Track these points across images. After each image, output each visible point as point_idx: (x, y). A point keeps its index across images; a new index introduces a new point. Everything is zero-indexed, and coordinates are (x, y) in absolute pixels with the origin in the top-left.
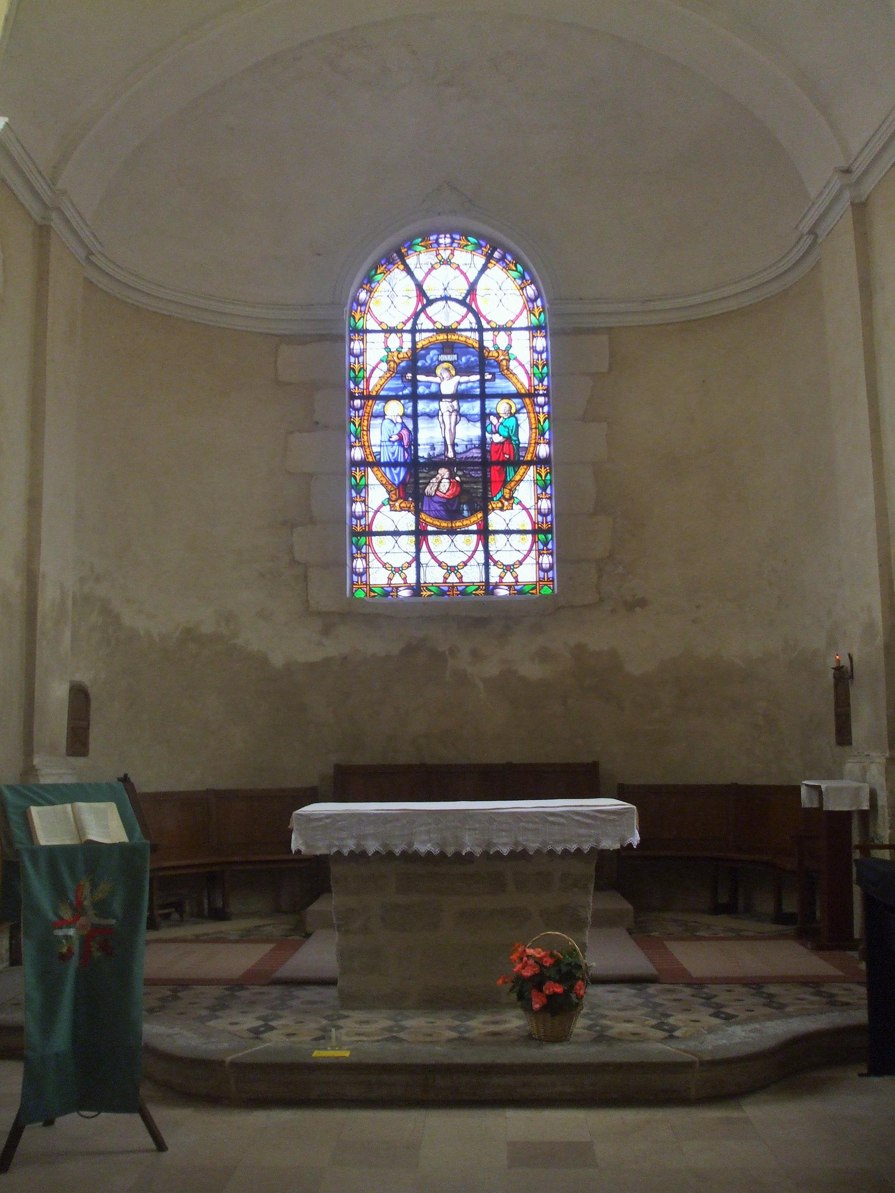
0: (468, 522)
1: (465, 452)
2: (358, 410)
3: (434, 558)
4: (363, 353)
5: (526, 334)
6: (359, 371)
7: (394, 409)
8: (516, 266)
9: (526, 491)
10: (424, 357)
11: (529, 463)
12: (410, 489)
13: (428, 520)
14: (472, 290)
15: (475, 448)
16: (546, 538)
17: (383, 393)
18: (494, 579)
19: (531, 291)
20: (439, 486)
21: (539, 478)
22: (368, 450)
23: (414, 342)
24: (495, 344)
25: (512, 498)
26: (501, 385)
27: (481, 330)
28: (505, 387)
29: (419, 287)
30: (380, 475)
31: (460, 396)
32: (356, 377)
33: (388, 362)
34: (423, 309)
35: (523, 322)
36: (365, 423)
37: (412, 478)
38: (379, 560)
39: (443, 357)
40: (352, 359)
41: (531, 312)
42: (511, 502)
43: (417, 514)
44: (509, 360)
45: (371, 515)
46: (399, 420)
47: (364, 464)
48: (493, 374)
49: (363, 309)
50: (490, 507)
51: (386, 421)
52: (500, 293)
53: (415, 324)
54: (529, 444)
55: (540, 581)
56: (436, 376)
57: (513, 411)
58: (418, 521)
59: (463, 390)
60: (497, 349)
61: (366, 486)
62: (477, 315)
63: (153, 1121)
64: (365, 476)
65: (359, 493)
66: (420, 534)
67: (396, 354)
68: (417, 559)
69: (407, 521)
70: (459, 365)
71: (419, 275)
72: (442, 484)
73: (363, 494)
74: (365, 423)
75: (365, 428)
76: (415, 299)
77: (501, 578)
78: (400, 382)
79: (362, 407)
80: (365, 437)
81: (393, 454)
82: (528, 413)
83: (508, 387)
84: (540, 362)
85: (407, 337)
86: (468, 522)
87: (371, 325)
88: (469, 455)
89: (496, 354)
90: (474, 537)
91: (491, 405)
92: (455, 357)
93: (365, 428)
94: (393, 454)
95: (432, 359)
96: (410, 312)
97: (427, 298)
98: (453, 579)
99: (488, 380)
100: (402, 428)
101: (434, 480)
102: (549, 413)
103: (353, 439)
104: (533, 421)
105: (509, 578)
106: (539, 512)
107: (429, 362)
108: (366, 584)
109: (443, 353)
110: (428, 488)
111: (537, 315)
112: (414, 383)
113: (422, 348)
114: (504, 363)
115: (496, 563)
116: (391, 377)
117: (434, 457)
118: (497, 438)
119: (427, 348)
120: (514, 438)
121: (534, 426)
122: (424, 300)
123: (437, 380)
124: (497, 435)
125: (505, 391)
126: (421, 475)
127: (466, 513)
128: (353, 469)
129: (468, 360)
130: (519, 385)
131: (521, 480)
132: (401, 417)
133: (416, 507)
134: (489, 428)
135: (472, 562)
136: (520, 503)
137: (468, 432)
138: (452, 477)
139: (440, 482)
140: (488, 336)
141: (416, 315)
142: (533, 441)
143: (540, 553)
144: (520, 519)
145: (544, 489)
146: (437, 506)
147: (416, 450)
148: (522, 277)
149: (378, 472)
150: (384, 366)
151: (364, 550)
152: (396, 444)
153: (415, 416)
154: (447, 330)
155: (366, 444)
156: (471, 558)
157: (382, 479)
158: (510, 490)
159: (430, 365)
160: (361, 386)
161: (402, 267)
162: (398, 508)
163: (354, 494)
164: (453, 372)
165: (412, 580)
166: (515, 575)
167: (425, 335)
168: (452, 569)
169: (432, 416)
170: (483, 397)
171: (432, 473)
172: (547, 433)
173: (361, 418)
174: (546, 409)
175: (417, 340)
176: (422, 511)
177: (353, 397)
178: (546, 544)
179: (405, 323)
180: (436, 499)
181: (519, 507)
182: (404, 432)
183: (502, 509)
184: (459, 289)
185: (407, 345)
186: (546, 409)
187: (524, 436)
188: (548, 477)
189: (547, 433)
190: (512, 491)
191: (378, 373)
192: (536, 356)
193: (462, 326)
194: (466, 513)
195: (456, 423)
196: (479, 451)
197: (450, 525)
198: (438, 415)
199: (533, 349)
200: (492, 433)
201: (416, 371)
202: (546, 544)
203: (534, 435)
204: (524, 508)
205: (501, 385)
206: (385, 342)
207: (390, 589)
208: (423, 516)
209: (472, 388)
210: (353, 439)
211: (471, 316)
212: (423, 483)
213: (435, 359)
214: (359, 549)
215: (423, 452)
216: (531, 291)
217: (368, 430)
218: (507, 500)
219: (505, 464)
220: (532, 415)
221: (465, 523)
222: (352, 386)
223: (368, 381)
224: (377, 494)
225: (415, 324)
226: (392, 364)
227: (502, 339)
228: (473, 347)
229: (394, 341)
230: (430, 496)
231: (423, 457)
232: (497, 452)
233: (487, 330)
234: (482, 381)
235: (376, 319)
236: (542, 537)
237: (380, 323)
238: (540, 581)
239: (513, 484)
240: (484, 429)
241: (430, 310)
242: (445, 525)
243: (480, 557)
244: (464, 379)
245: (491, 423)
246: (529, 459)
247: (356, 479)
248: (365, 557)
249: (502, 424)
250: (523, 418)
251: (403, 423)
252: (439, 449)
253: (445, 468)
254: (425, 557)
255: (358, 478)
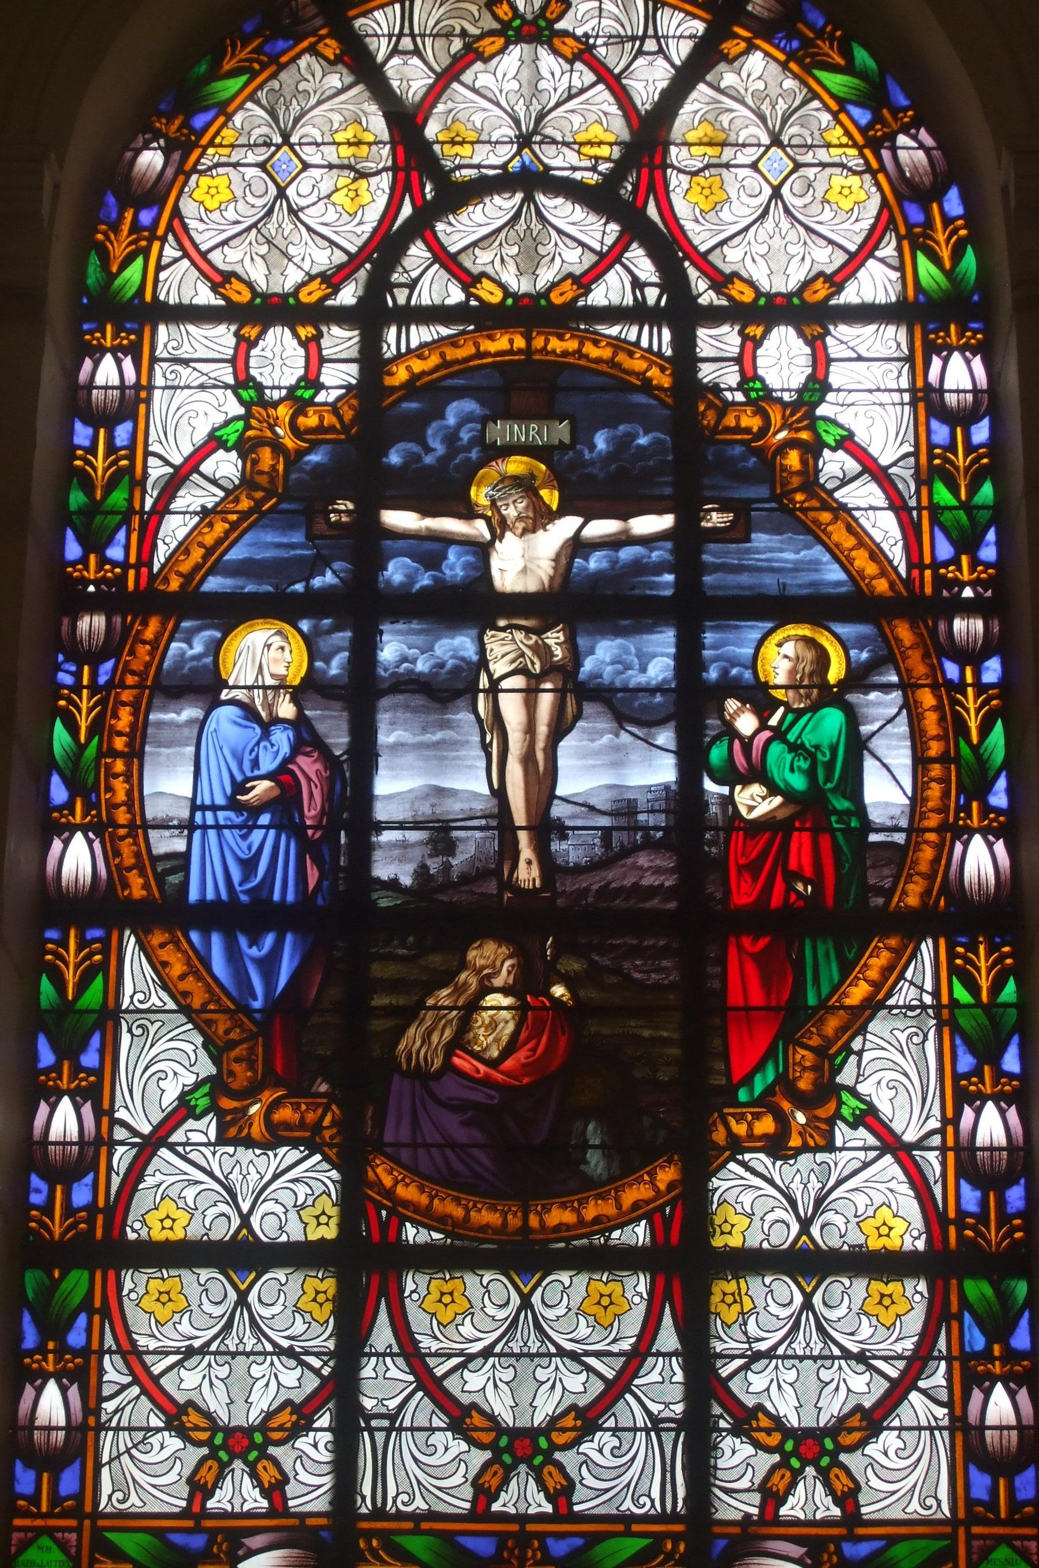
0: (608, 1208)
1: (595, 866)
2: (95, 659)
3: (430, 1385)
4: (133, 402)
5: (890, 339)
6: (111, 486)
7: (262, 655)
8: (847, 53)
9: (894, 1069)
10: (414, 429)
11: (911, 927)
12: (315, 1047)
13: (408, 1192)
14: (648, 138)
15: (649, 845)
16: (1004, 1297)
17: (214, 584)
18: (736, 1506)
19: (911, 152)
20: (465, 1024)
21: (961, 994)
22: (127, 848)
23: (370, 359)
24: (749, 377)
25: (828, 1090)
26: (777, 554)
27: (683, 315)
28: (797, 568)
29: (405, 122)
30: (177, 969)
31: (576, 602)
32: (94, 508)
33: (245, 448)
34: (421, 226)
35: (875, 283)
36: (125, 719)
37: (333, 987)
38: (150, 1386)
39: (502, 431)
40: (82, 433)
41: (917, 240)
42: (825, 1111)
43: (351, 1163)
44: (813, 449)
45: (122, 1157)
46: (286, 709)
47: (101, 910)
48: (741, 509)
49: (146, 217)
50: (720, 1136)
51: (225, 714)
52: (777, 162)
53: (379, 285)
54: (913, 830)
55: (973, 1519)
56: (469, 513)
57: (836, 672)
58: (353, 1198)
59: (598, 576)
60: (761, 399)
61: (109, 1016)
62: (669, 248)
63: (452, 533)
64: (106, 967)
65: (69, 1050)
66: (361, 1268)
67: (283, 412)
68: (341, 1388)
69: (293, 1193)
70: (580, 463)
71: (410, 78)
72: (490, 1013)
73: (90, 1059)
74: (125, 719)
75: (119, 743)
76: (385, 181)
77: (772, 1496)
78: (297, 537)
79: (112, 646)
80: (120, 787)
81: (249, 865)
82: (907, 686)
83: (814, 565)
84: (961, 460)
85: (341, 340)
86: (608, 1208)
87: (182, 284)
88: (617, 877)
89: (751, 421)
90: (638, 1286)
91: (728, 646)
92: (562, 431)
93: (119, 743)
94: (249, 865)
95: (451, 438)
96: (355, 234)
97: (441, 176)
98: (523, 1496)
99: (716, 535)
100: (296, 749)
101: (444, 995)
102: (1004, 684)
103: (59, 793)
104: (931, 722)
105: (808, 1501)
106: (965, 1158)
107: (439, 448)
108: (77, 1512)
109: (509, 414)
110: (413, 1033)
111: (945, 254)
112: (369, 544)
113: (412, 387)
114: (793, 459)
115: (748, 1421)
116: (255, 518)
117: (449, 886)
118: (754, 802)
119: (432, 386)
120: (841, 804)
121: (935, 749)
122: (426, 181)
123: (480, 529)
124: (757, 789)
125: (797, 584)
126: (378, 970)
127: (595, 1162)
128: (52, 934)
129: (622, 445)
130: (861, 560)
131: (873, 1006)
132: (298, 695)
133: (347, 1126)
134: (717, 755)
135: (629, 1411)
136: (868, 1117)
137: (611, 770)
138: (526, 987)
139: (473, 1006)
140: (717, 341)
141: (385, 248)
142: (933, 820)
143: (971, 1376)
144: (878, 1204)
145: (988, 1053)
146: (453, 1124)
147: (363, 852)
148: (874, 97)
149: (167, 954)
150: (225, 465)
151: (76, 1338)
152: (265, 819)
153: (362, 692)
154: (527, 312)
155: (122, 816)
156: (617, 1388)
157: (190, 984)
158: (820, 1052)
159: (444, 460)
160: (115, 553)
161: (331, 47)
162: (257, 1130)
163: (47, 1057)
164: (551, 497)
165: (310, 1489)
166: (842, 1484)
167: (420, 335)
168: (517, 1448)
169: (448, 691)
170: (693, 610)
171: (435, 959)
172: (1002, 783)
173: (105, 695)
174: (992, 670)
175: (389, 350)
176: (379, 1147)
177: (74, 600)
178: (998, 1328)
179: (333, 279)
180: (449, 1088)
181: (864, 1136)
182: (308, 765)
183: (777, 1147)
184: (589, 128)
185: (338, 376)
186: (992, 670)
187: (886, 791)
188: (1010, 991)
189: (1002, 783)
190: (830, 1058)
191: (191, 498)
192: (941, 432)
193: (599, 296)
194: (595, 1162)
195: (560, 729)
196: (666, 861)
197: (514, 1221)
198: (473, 690)
199: (926, 399)
200: (732, 777)
201: (383, 488)
202: (998, 1328)
203: (935, 791)
204: (891, 1144)
205: (777, 554)
206: (239, 360)
207: (198, 1542)
208: (383, 1173)
209: (638, 567)
210: (59, 793)
211: (641, 263)
212: (388, 1011)
213: (465, 436)
214: (53, 1327)
215: (393, 865)
216: (911, 152)
217: (135, 754)
218: (802, 1101)
219: (788, 927)
220: (928, 699)
221: (590, 1212)
222: (73, 550)
223: (149, 528)
224: (161, 1064)
225: (379, 285)
226: (266, 456)
227: (783, 359)
228: (647, 386)
229: (279, 359)
230: (420, 1075)
231: (393, 884)
232: (753, 868)
233: (714, 316)
234: (687, 539)
235: (200, 259)
236: (977, 1289)
237: (221, 280)
238: (973, 1519)
239: (832, 1024)
240: (692, 760)
241: (458, 230)
242: (487, 1217)
243: (663, 1385)
244: (601, 528)
245: (730, 732)
246: (913, 901)
247: (59, 983)
248: (81, 1374)
249: (779, 734)
250: (881, 706)
251: (300, 724)
252: (471, 846)
253: (501, 939)
254: (383, 1383)
255: (71, 978)
